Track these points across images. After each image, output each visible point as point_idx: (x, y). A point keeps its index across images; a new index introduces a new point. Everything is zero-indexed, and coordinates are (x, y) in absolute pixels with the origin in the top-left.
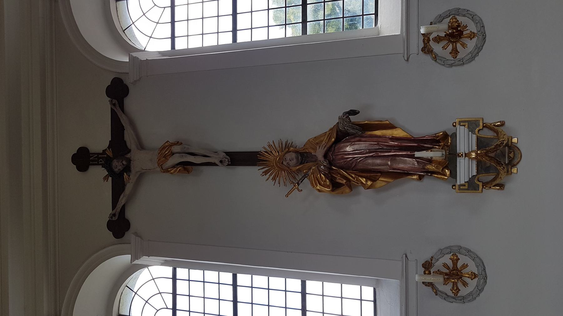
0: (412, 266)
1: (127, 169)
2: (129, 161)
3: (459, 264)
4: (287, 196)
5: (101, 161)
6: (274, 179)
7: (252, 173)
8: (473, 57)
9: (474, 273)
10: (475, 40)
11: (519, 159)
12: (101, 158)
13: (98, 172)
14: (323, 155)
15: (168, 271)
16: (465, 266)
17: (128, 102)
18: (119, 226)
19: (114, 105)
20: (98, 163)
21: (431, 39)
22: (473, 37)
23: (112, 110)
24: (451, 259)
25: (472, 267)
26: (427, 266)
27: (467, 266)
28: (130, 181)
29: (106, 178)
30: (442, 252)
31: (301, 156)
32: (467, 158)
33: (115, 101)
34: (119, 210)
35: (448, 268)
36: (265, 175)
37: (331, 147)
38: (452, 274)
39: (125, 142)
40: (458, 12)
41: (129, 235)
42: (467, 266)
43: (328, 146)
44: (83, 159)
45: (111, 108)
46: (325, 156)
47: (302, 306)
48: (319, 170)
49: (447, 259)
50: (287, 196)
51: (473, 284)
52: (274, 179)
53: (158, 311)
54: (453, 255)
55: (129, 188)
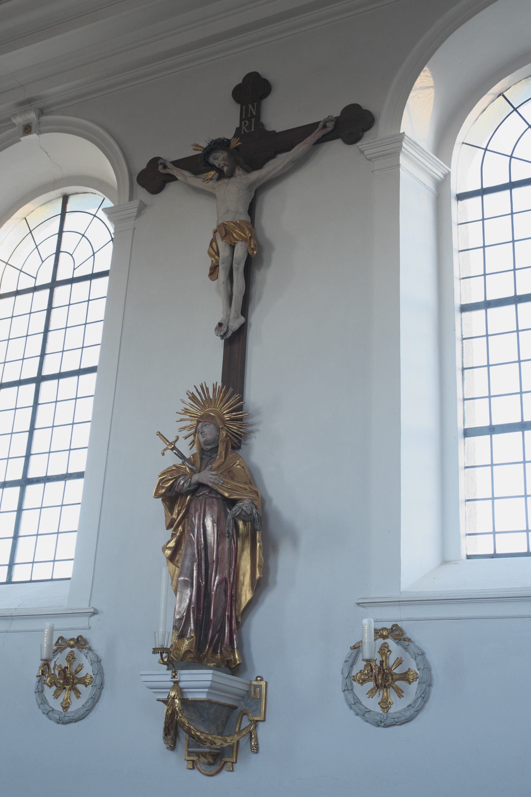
0: (81, 622)
1: (221, 175)
2: (231, 175)
3: (80, 687)
4: (159, 434)
5: (245, 123)
6: (186, 411)
7: (213, 375)
8: (355, 704)
9: (68, 707)
10: (379, 710)
11: (203, 771)
12: (250, 122)
13: (226, 122)
14: (200, 481)
15: (104, 262)
16: (78, 693)
17: (337, 145)
18: (153, 178)
19: (325, 126)
20: (244, 119)
21: (386, 641)
22: (381, 707)
23: (316, 124)
24: (87, 674)
25: (77, 705)
26: (80, 643)
27: (78, 697)
28: (205, 183)
29: (196, 146)
30: (98, 661)
31: (212, 449)
32: (172, 684)
33: (330, 126)
34: (171, 172)
35: (77, 672)
36: (190, 398)
37: (218, 493)
38: (67, 674)
39: (273, 156)
40: (427, 685)
41: (142, 193)
42: (78, 697)
43: (216, 488)
44: (252, 91)
45: (319, 122)
46: (200, 485)
47: (71, 474)
48: (179, 477)
49: (87, 670)
50: (159, 434)
51: (56, 704)
52: (186, 411)
53: (71, 255)
54: (91, 677)
55: (197, 182)
